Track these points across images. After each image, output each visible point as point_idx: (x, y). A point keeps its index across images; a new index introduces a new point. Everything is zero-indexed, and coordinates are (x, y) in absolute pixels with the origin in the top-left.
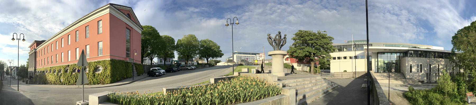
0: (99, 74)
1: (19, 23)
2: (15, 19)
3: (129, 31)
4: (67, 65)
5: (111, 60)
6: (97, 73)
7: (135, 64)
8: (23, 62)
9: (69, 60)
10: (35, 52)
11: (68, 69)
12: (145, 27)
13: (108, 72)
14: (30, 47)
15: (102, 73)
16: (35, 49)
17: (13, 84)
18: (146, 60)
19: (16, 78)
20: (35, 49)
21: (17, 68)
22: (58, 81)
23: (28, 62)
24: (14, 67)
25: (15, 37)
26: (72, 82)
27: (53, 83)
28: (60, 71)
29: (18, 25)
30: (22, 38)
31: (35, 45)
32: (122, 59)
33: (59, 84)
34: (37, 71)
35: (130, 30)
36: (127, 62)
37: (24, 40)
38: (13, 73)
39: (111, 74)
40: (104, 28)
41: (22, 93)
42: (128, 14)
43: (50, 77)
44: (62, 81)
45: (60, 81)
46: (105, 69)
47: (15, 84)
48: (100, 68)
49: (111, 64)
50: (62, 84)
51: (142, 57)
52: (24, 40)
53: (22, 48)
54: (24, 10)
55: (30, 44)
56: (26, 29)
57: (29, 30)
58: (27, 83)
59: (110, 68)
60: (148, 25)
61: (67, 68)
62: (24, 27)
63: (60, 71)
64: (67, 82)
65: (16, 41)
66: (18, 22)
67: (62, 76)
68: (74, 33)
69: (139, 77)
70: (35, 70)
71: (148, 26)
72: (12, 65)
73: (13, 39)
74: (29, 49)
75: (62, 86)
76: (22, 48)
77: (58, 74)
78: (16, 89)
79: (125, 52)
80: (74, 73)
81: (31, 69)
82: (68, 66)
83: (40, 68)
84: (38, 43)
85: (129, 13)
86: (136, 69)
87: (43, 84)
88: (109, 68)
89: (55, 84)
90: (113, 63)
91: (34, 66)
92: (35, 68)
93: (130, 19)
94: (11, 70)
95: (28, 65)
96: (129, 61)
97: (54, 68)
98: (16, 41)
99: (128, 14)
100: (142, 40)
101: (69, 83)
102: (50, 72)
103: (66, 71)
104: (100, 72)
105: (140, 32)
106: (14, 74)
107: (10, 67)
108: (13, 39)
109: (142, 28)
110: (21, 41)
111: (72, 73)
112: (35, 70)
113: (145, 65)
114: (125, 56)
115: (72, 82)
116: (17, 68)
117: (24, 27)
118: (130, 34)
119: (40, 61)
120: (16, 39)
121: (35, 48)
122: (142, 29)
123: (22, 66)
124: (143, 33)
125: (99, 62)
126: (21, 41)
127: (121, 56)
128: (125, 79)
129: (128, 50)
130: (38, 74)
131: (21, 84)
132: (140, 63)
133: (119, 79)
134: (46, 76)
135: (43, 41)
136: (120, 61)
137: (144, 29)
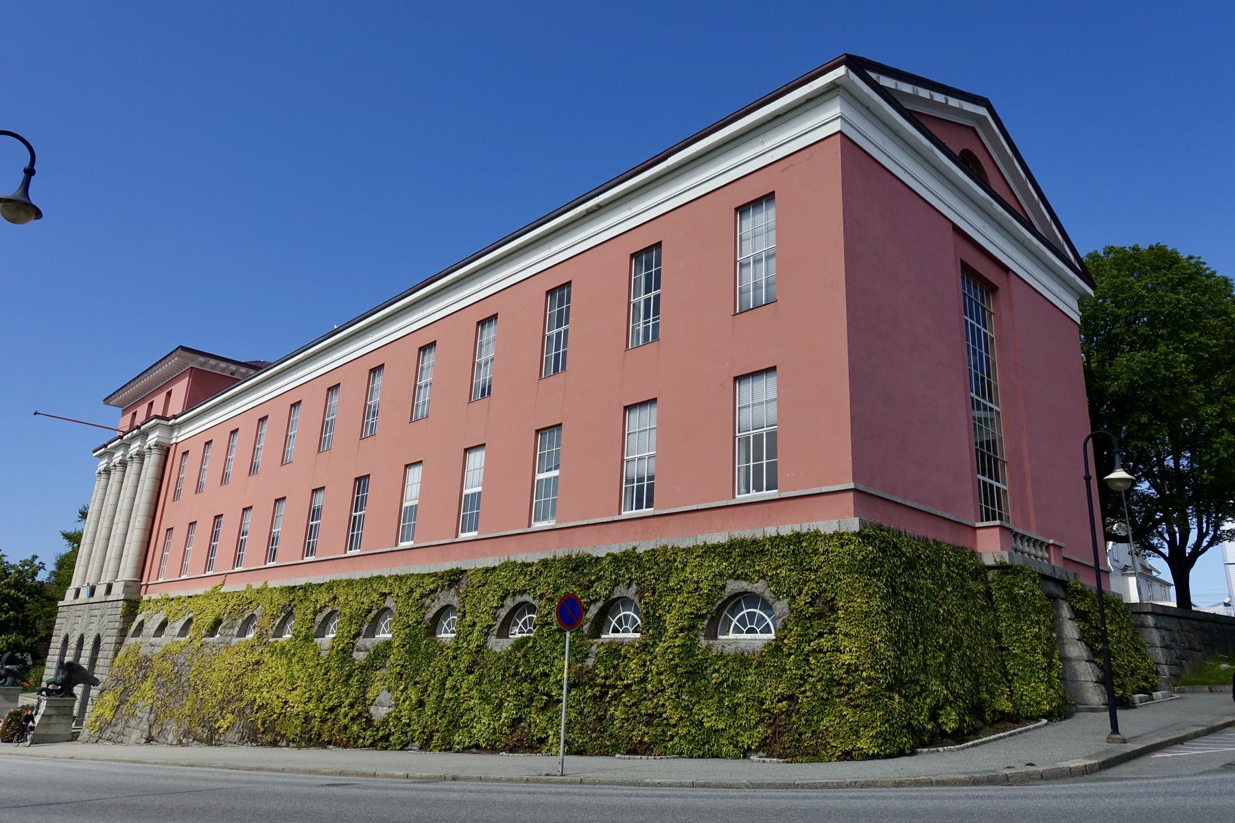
4: (448, 566)
13: (851, 646)
27: (294, 728)
44: (379, 713)
50: (382, 743)
82: (454, 578)
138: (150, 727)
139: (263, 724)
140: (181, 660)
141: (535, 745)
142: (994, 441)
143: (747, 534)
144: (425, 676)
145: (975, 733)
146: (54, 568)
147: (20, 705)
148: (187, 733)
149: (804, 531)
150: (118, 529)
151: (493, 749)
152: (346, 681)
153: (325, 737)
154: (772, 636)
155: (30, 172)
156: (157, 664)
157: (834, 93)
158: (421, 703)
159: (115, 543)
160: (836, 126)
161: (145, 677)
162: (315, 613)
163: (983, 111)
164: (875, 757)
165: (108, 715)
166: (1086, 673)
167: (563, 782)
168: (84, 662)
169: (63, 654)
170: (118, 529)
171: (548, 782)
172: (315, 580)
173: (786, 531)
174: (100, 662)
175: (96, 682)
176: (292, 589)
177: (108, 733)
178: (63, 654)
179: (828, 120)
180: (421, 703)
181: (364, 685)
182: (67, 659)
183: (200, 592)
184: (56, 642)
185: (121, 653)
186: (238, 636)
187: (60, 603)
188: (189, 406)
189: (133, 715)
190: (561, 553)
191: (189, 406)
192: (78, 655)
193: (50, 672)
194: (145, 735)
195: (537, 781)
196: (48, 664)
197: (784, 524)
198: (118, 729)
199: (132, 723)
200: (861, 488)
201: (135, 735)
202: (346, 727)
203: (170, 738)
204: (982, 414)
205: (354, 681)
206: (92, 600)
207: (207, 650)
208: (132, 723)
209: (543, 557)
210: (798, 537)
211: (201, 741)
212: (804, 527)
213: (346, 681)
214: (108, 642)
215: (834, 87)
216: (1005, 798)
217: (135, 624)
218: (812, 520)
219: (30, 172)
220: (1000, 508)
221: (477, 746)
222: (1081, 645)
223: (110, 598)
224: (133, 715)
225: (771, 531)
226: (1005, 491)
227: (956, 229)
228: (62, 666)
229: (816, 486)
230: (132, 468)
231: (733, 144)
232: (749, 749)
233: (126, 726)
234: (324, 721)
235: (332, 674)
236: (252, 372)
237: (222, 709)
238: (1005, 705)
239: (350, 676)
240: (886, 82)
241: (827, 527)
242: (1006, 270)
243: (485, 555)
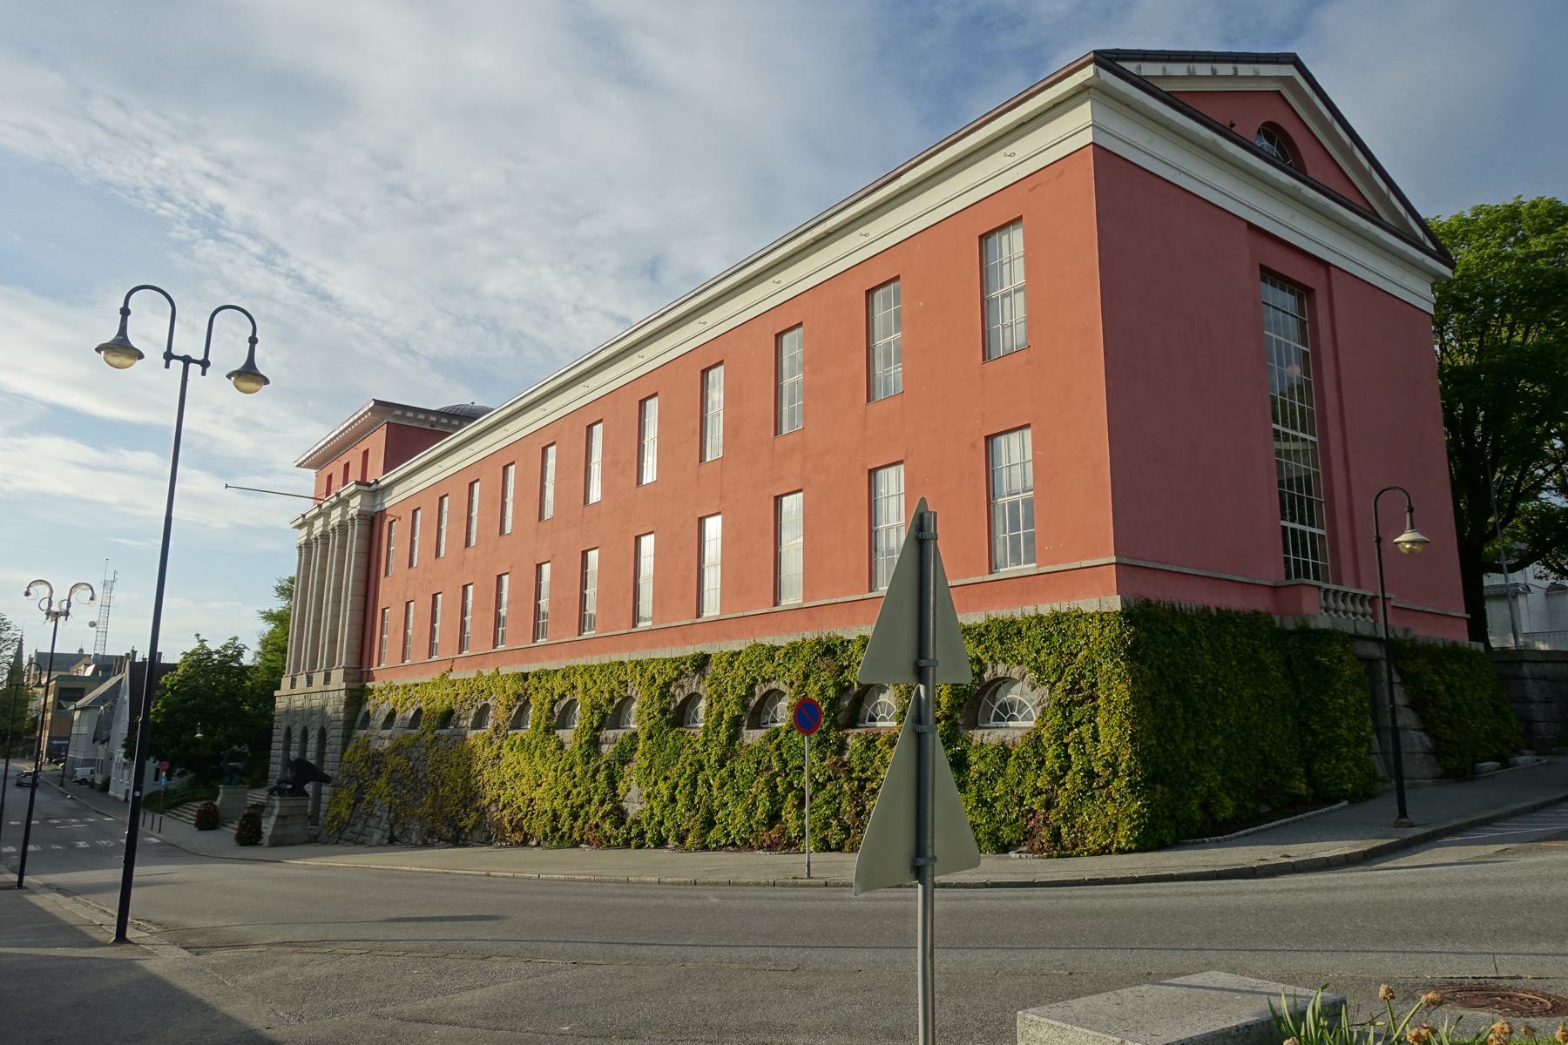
0: (1004, 752)
1: (218, 209)
2: (181, 160)
3: (1287, 300)
4: (691, 650)
5: (1129, 615)
6: (987, 737)
7: (1396, 650)
8: (221, 614)
9: (712, 609)
10: (373, 523)
11: (693, 698)
12: (1464, 230)
13: (1110, 733)
14: (319, 461)
15: (1036, 741)
16: (375, 492)
17: (71, 857)
18: (1509, 595)
19: (122, 784)
20: (375, 492)
21: (148, 672)
22: (595, 812)
23: (280, 619)
24: (106, 666)
25: (147, 330)
26: (735, 817)
27: (539, 826)
28: (612, 714)
29: (212, 224)
30: (229, 354)
31: (377, 442)
32: (1236, 602)
33: (606, 842)
34: (378, 706)
35: (1304, 293)
36: (1307, 634)
37: (249, 374)
38: (81, 724)
39: (1143, 756)
40: (1041, 298)
41: (166, 961)
42: (1272, 131)
43: (516, 774)
44: (634, 807)
45: (619, 815)
46: (1075, 700)
47: (94, 858)
48: (1014, 694)
49: (1134, 654)
50: (636, 840)
51: (1474, 564)
52: (249, 374)
53: (216, 465)
54: (297, 97)
55: (319, 435)
56: (298, 279)
57: (325, 297)
58: (249, 835)
59: (1121, 692)
60: (1499, 198)
61: (691, 685)
62: (266, 261)
63: (612, 714)
64: (693, 823)
65: (152, 379)
66: (215, 194)
67: (639, 761)
68: (759, 380)
69: (1463, 799)
70: (357, 696)
71: (1513, 214)
72: (74, 638)
73: (121, 348)
74: (309, 480)
75: (632, 856)
76: (216, 465)
77: (595, 743)
78: (98, 914)
79: (1270, 521)
80: (752, 737)
81: (311, 691)
82: (702, 662)
83: (405, 678)
84: (409, 431)
85: (1284, 124)
86: (1416, 705)
87: (430, 839)
88: (1115, 690)
89: (558, 837)
90: (1158, 638)
91: (343, 656)
92: (359, 674)
93: (1298, 171)
94: (70, 692)
95: (275, 647)
96: (1323, 622)
97: (558, 685)
98: (152, 379)
99: (1272, 131)
100: (1455, 382)
101: (706, 831)
102: (517, 723)
103: (680, 716)
104: (1018, 729)
105: (1420, 294)
106: (101, 736)
107: (48, 661)
108: (121, 348)
109: (1438, 243)
110: (212, 388)
111: (734, 737)
112: (357, 696)
113: (1515, 659)
114: (1272, 573)
115: (735, 817)
116: (136, 668)
117: (271, 256)
118: (1307, 331)
119: (419, 611)
120: (154, 355)
121: (375, 472)
122: (1443, 255)
123: (200, 662)
124: (1450, 298)
125: (1007, 632)
126: (212, 388)
127: (1237, 568)
128: (1295, 805)
129: (1296, 499)
130: (383, 742)
131: (171, 851)
132: (1460, 635)
133: (1227, 808)
134: (468, 758)
135: (462, 416)
136: (1225, 618)
137: (1465, 255)
138: (392, 826)
139: (511, 822)
140: (416, 755)
141: (791, 845)
142: (1308, 478)
143: (1004, 613)
144: (673, 772)
145: (1258, 819)
146: (258, 648)
147: (249, 803)
148: (431, 833)
149: (1064, 610)
150: (327, 611)
151: (747, 846)
152: (593, 776)
153: (576, 835)
154: (1031, 724)
155: (253, 341)
156: (393, 761)
157: (1084, 95)
158: (673, 800)
159: (326, 626)
160: (1087, 137)
161: (379, 773)
162: (554, 702)
163: (1289, 70)
164: (1130, 851)
165: (345, 814)
166: (1415, 740)
167: (809, 885)
168: (311, 756)
169: (287, 749)
170: (327, 611)
171: (795, 885)
172: (551, 666)
173: (1045, 610)
174: (328, 757)
175: (327, 779)
176: (525, 677)
177: (347, 834)
178: (287, 749)
179: (1074, 130)
180: (673, 800)
181: (612, 782)
182: (294, 754)
183: (427, 679)
184: (278, 736)
185: (350, 749)
186: (474, 727)
187: (276, 693)
188: (388, 467)
189: (371, 815)
190: (811, 636)
191: (388, 467)
192: (304, 750)
193: (276, 769)
194: (387, 835)
195: (784, 885)
196: (273, 759)
197: (1044, 602)
198: (358, 829)
199: (372, 822)
200: (1125, 561)
201: (376, 837)
202: (597, 826)
203: (414, 838)
204: (1284, 446)
205: (601, 776)
206: (311, 689)
207: (442, 744)
208: (372, 822)
209: (791, 640)
210: (1057, 618)
211: (447, 841)
212: (1063, 607)
213: (593, 776)
214: (334, 735)
215: (1082, 91)
216: (1281, 891)
217: (361, 716)
218: (1073, 597)
219: (253, 341)
220: (1315, 557)
221: (733, 844)
222: (1410, 712)
223: (330, 687)
224: (371, 815)
225: (1030, 611)
226: (1322, 536)
227: (1252, 227)
228: (288, 764)
229: (1076, 560)
230: (334, 543)
231: (971, 159)
232: (1010, 843)
233: (366, 825)
234: (575, 817)
235: (578, 770)
236: (456, 423)
237: (465, 806)
238: (1302, 788)
239: (597, 770)
240: (1150, 69)
241: (1089, 605)
242: (1326, 265)
243: (730, 637)
